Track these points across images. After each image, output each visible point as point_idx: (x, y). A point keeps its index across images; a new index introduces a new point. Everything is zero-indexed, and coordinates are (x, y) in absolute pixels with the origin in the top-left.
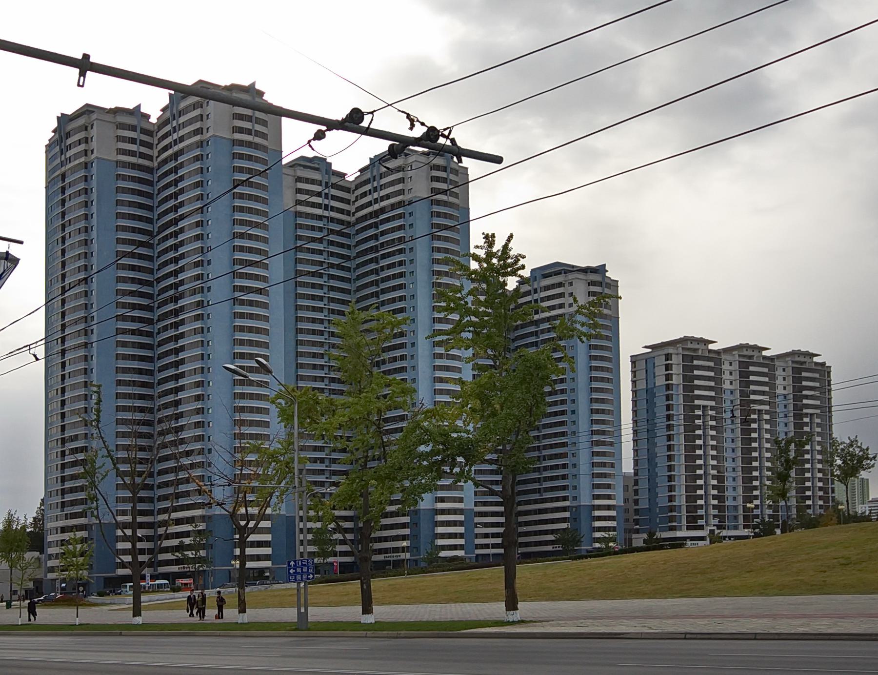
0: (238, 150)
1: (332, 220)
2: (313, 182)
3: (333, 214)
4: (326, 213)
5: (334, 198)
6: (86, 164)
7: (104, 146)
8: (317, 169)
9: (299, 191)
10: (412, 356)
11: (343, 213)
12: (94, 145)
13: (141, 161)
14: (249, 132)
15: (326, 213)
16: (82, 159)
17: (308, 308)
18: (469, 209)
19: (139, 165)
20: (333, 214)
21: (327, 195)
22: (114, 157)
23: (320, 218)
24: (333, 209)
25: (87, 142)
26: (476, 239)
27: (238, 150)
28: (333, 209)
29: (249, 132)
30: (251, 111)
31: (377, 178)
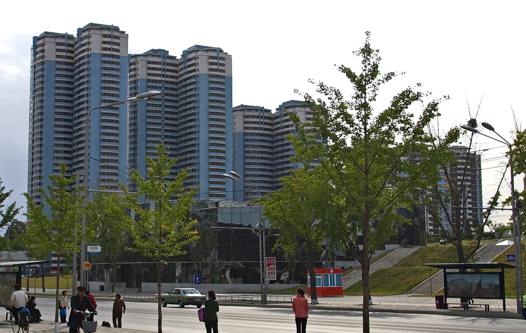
0: (104, 59)
1: (167, 82)
2: (156, 63)
3: (167, 79)
4: (163, 79)
5: (168, 70)
6: (42, 62)
7: (51, 53)
8: (159, 56)
9: (149, 68)
10: (198, 163)
11: (173, 78)
12: (46, 54)
13: (67, 60)
14: (110, 49)
15: (163, 79)
16: (41, 60)
17: (153, 136)
18: (232, 77)
19: (66, 62)
20: (167, 79)
21: (164, 69)
22: (55, 59)
23: (160, 82)
24: (167, 76)
25: (43, 52)
26: (12, 298)
27: (104, 59)
28: (167, 76)
29: (110, 49)
30: (114, 36)
31: (186, 61)
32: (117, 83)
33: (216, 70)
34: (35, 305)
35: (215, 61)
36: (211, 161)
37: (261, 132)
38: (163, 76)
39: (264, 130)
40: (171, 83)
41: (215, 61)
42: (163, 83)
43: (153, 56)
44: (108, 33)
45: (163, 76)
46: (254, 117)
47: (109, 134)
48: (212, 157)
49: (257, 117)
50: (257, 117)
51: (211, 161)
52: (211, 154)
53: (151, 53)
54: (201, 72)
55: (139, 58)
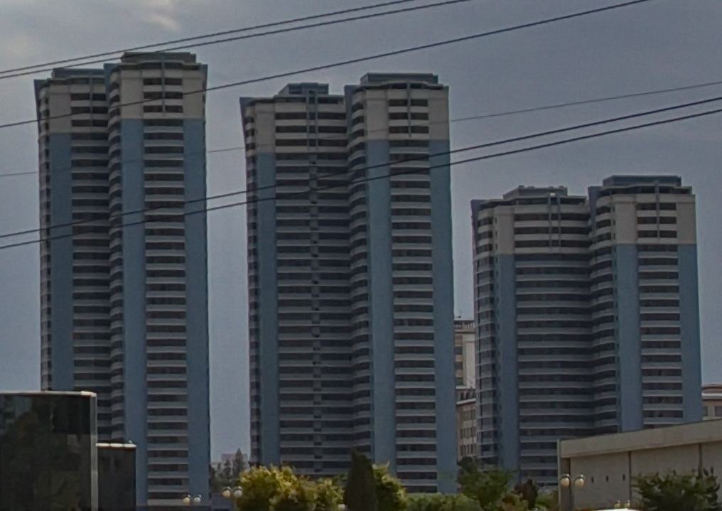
3: (323, 149)
4: (313, 150)
15: (313, 150)
20: (323, 149)
24: (321, 143)
32: (179, 178)
33: (405, 130)
34: (380, 475)
35: (402, 109)
36: (399, 330)
37: (556, 250)
38: (312, 143)
39: (563, 246)
40: (330, 156)
41: (402, 109)
42: (314, 159)
43: (288, 100)
44: (83, 89)
45: (312, 143)
46: (535, 217)
47: (163, 288)
48: (401, 323)
49: (545, 217)
50: (545, 217)
51: (399, 330)
52: (398, 316)
53: (287, 95)
54: (370, 137)
55: (259, 107)
